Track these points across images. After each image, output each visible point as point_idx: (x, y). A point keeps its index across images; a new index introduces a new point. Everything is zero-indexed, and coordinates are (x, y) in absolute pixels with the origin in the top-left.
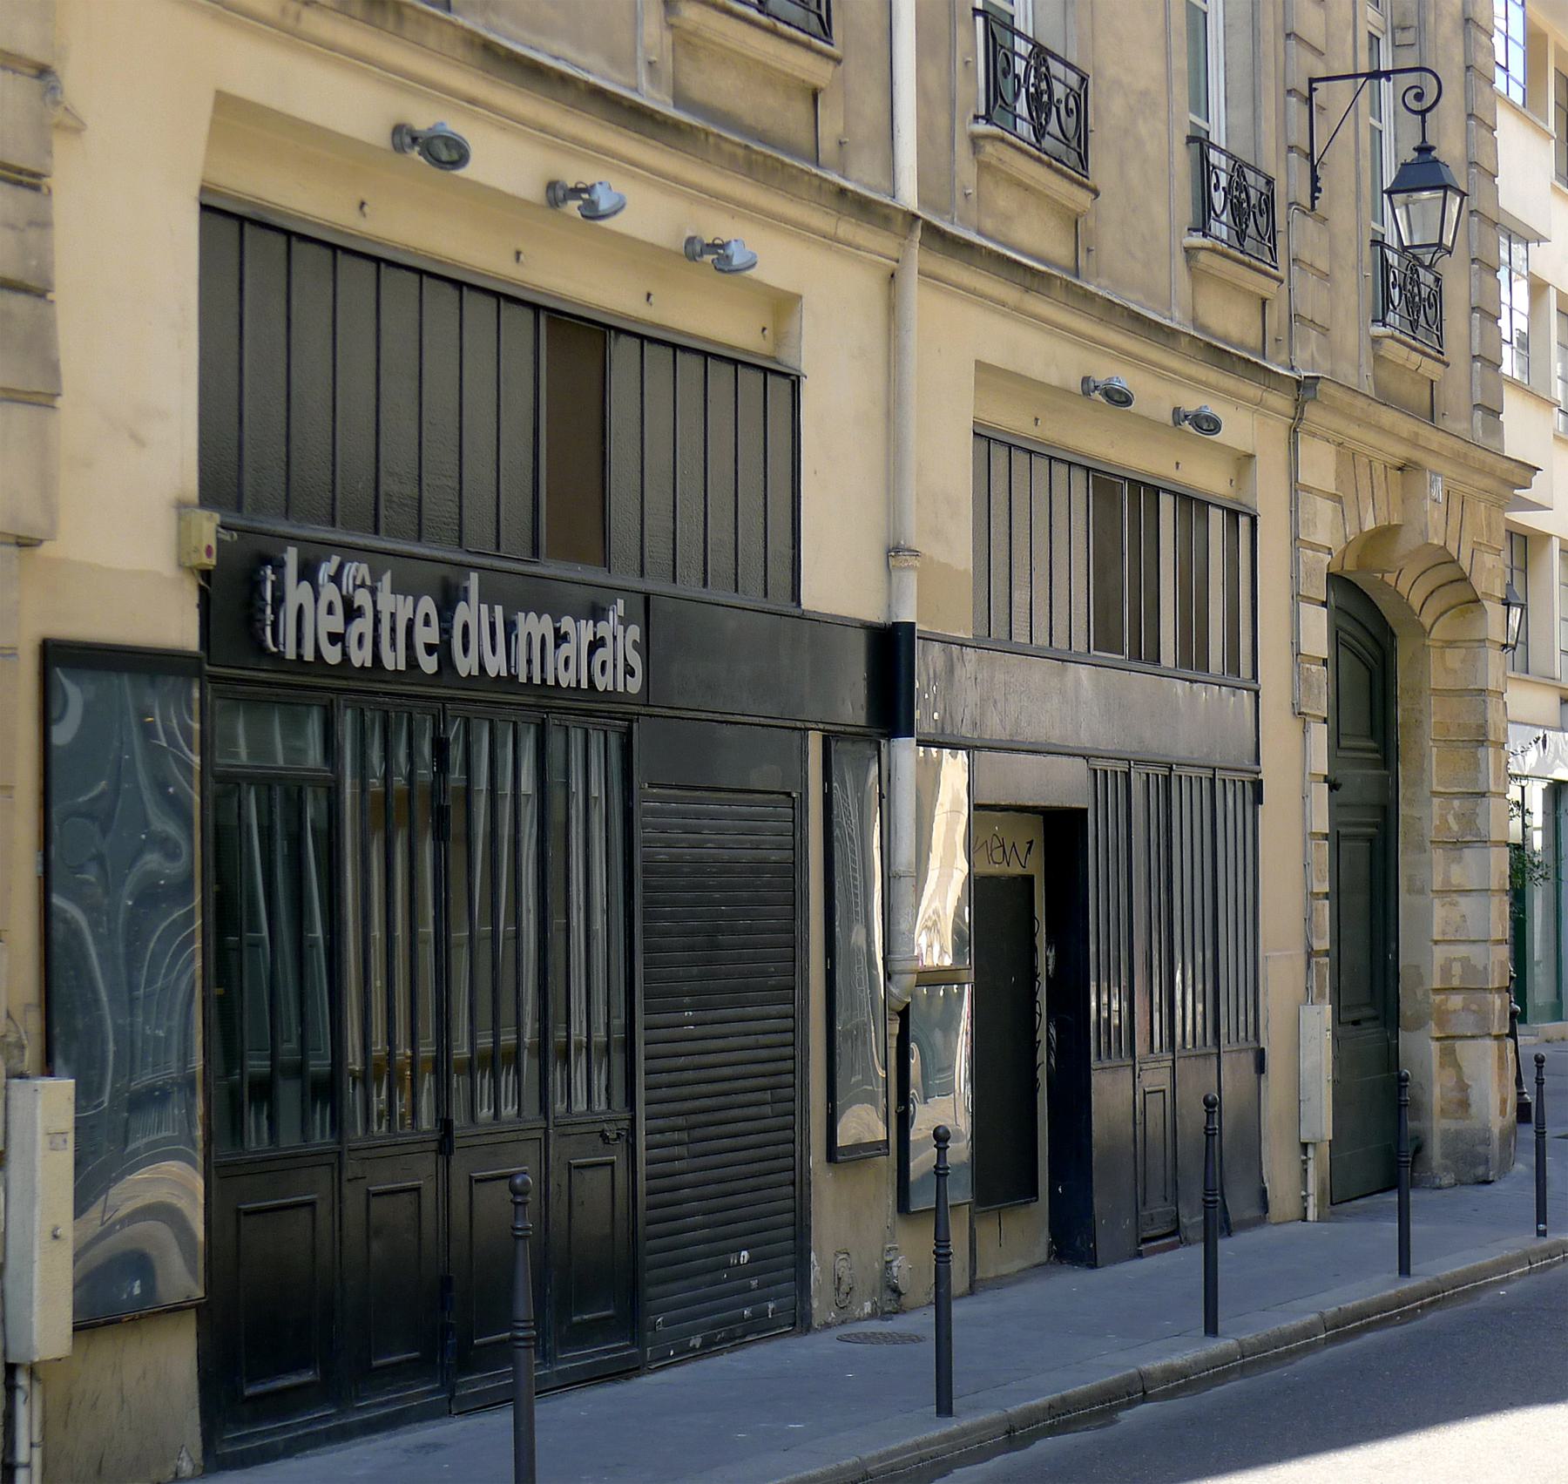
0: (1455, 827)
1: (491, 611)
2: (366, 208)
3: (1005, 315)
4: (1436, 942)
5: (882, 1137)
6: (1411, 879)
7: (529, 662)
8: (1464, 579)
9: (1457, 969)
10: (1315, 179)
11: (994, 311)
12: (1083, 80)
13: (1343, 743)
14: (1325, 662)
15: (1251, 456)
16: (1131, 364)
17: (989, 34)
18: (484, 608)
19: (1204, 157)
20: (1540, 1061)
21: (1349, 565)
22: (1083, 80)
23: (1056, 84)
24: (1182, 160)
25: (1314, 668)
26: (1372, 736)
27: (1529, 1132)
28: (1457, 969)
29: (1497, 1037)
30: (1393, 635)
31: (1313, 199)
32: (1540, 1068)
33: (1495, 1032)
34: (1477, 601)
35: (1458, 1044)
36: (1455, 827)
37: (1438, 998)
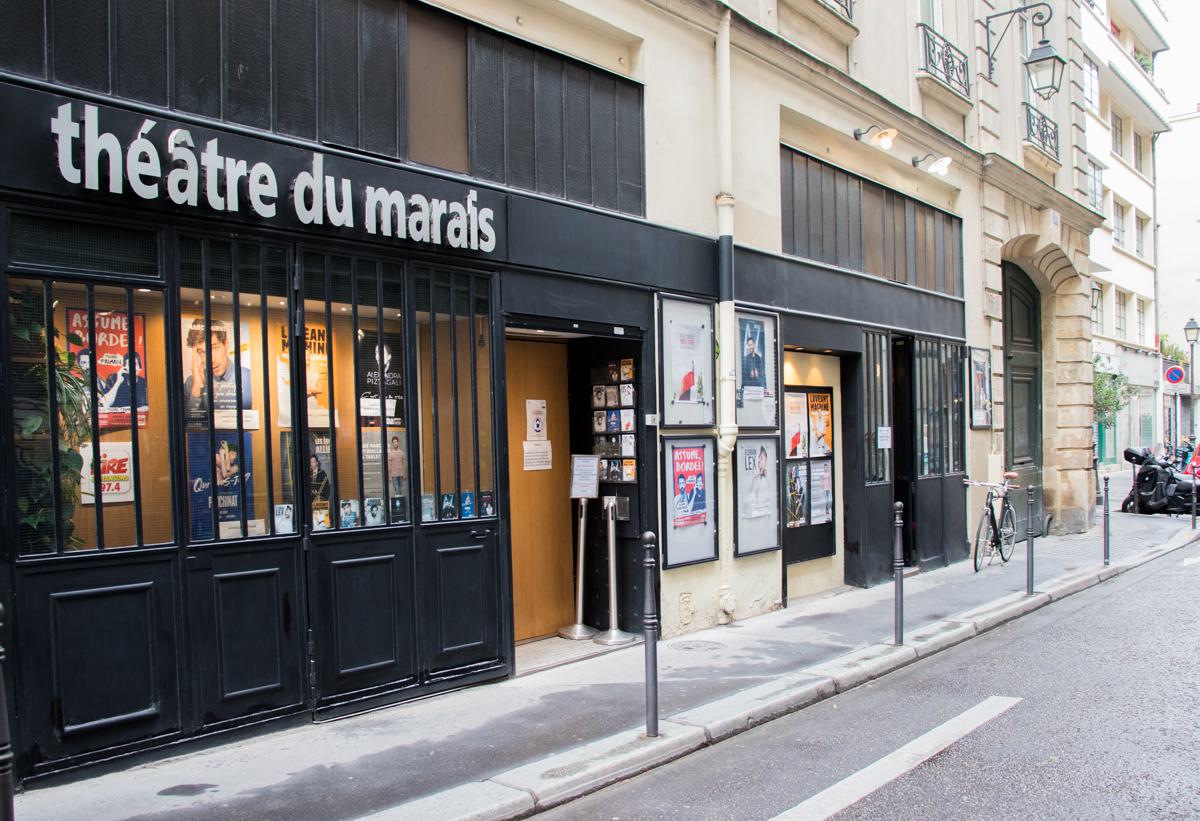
0: (1068, 377)
1: (338, 184)
2: (520, 21)
3: (800, 85)
4: (1059, 428)
5: (222, 537)
6: (1048, 400)
7: (867, 347)
8: (1071, 265)
9: (1069, 439)
10: (991, 65)
11: (792, 80)
12: (1056, 126)
13: (1015, 338)
14: (1000, 293)
15: (958, 190)
16: (826, 98)
17: (926, 34)
18: (330, 180)
19: (1028, 111)
20: (1106, 479)
21: (1015, 255)
22: (1056, 126)
23: (954, 59)
24: (1021, 113)
25: (995, 295)
26: (1029, 337)
27: (1100, 510)
28: (1069, 439)
29: (1088, 469)
30: (1038, 291)
31: (990, 73)
32: (1106, 483)
33: (1087, 467)
34: (1076, 276)
35: (1070, 473)
36: (1068, 377)
37: (1059, 452)
